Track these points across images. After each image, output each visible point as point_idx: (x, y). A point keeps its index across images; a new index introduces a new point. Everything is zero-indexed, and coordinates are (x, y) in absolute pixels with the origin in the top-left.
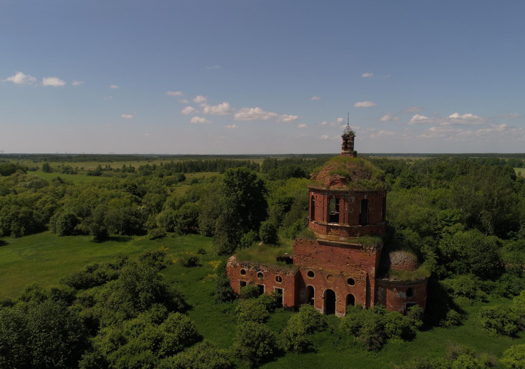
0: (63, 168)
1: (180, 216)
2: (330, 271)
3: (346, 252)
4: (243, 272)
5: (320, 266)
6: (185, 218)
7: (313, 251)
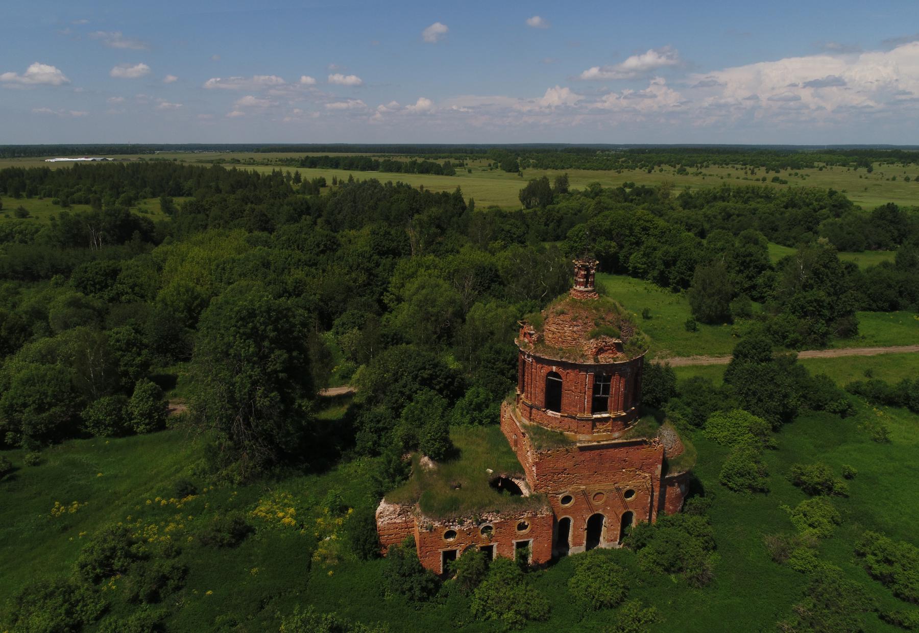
0: (742, 309)
1: (25, 405)
2: (597, 487)
3: (621, 453)
4: (451, 534)
5: (581, 484)
6: (40, 409)
7: (569, 464)
